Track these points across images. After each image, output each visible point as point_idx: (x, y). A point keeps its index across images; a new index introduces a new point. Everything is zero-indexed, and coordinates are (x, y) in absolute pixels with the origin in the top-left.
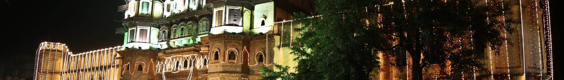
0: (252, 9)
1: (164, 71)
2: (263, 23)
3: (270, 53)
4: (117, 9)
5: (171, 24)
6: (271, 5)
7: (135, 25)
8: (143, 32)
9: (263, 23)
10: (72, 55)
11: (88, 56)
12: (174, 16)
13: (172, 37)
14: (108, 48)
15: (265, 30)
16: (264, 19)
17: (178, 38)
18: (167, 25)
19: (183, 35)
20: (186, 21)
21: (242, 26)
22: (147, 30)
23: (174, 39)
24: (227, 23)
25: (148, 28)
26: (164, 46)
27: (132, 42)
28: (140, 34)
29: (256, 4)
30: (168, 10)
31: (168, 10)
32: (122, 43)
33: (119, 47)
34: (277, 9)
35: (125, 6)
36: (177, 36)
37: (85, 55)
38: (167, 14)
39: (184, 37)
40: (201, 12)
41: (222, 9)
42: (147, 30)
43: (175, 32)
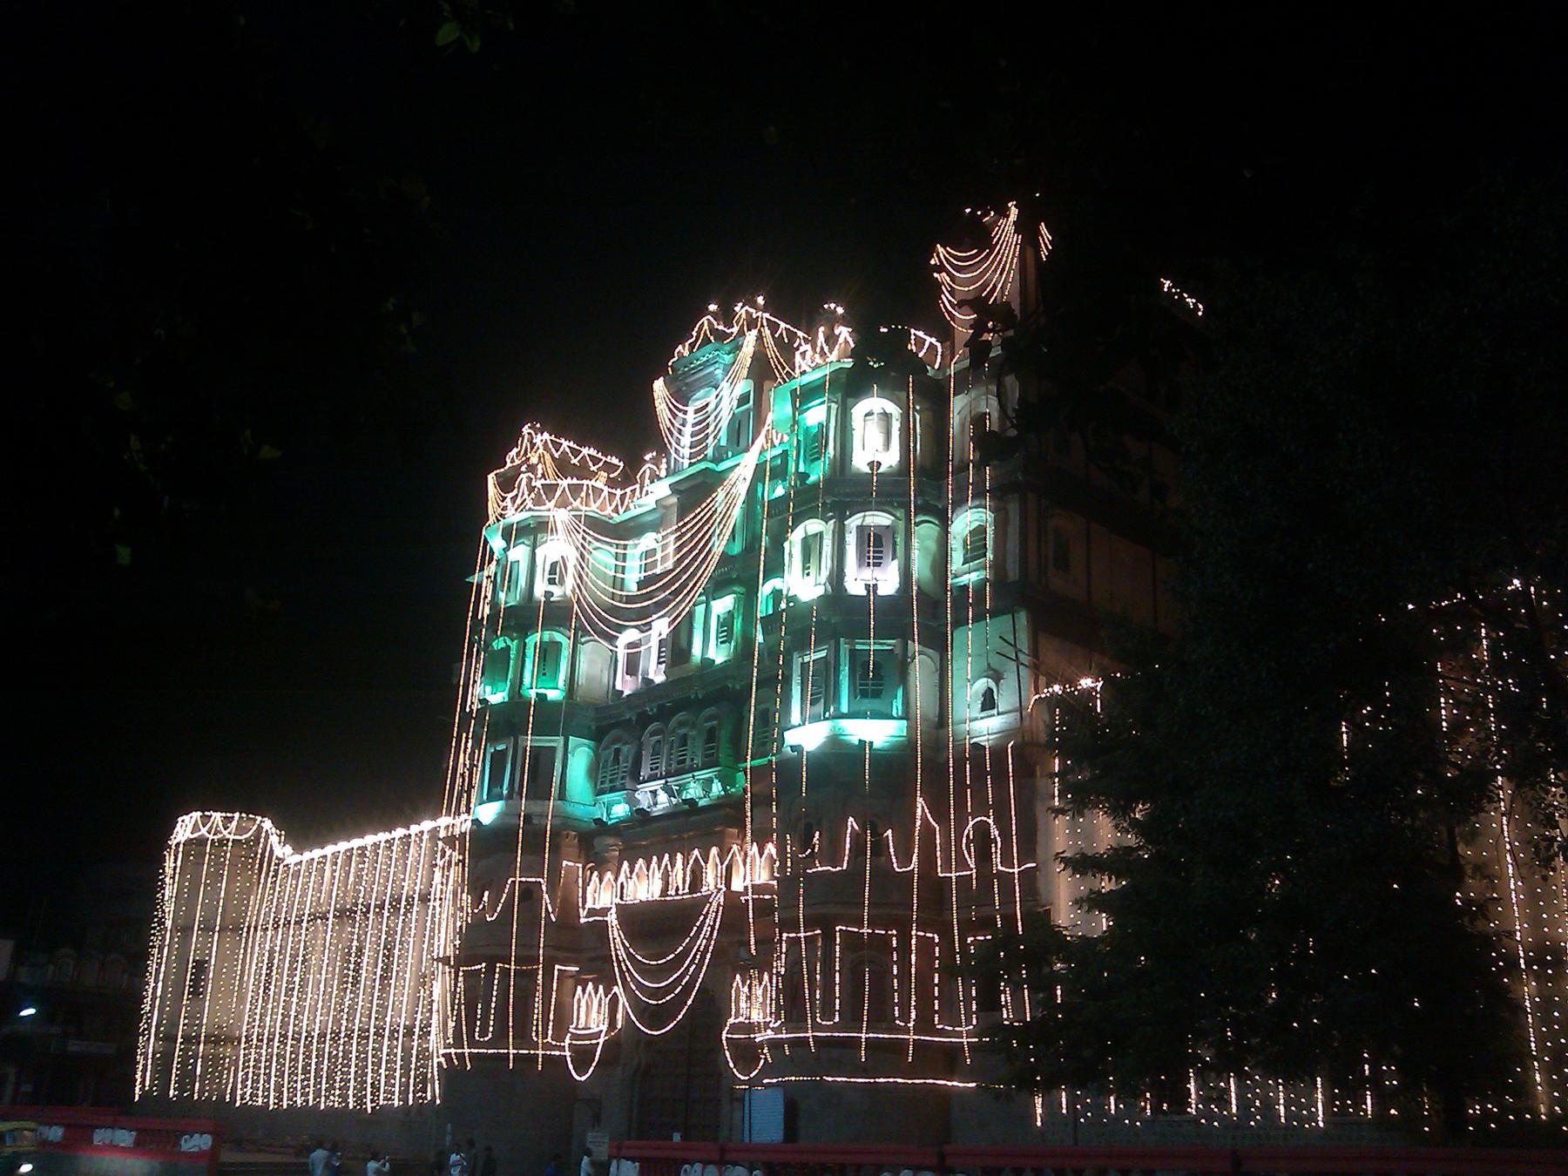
10: (292, 859)
16: (992, 685)
22: (554, 749)
42: (554, 749)
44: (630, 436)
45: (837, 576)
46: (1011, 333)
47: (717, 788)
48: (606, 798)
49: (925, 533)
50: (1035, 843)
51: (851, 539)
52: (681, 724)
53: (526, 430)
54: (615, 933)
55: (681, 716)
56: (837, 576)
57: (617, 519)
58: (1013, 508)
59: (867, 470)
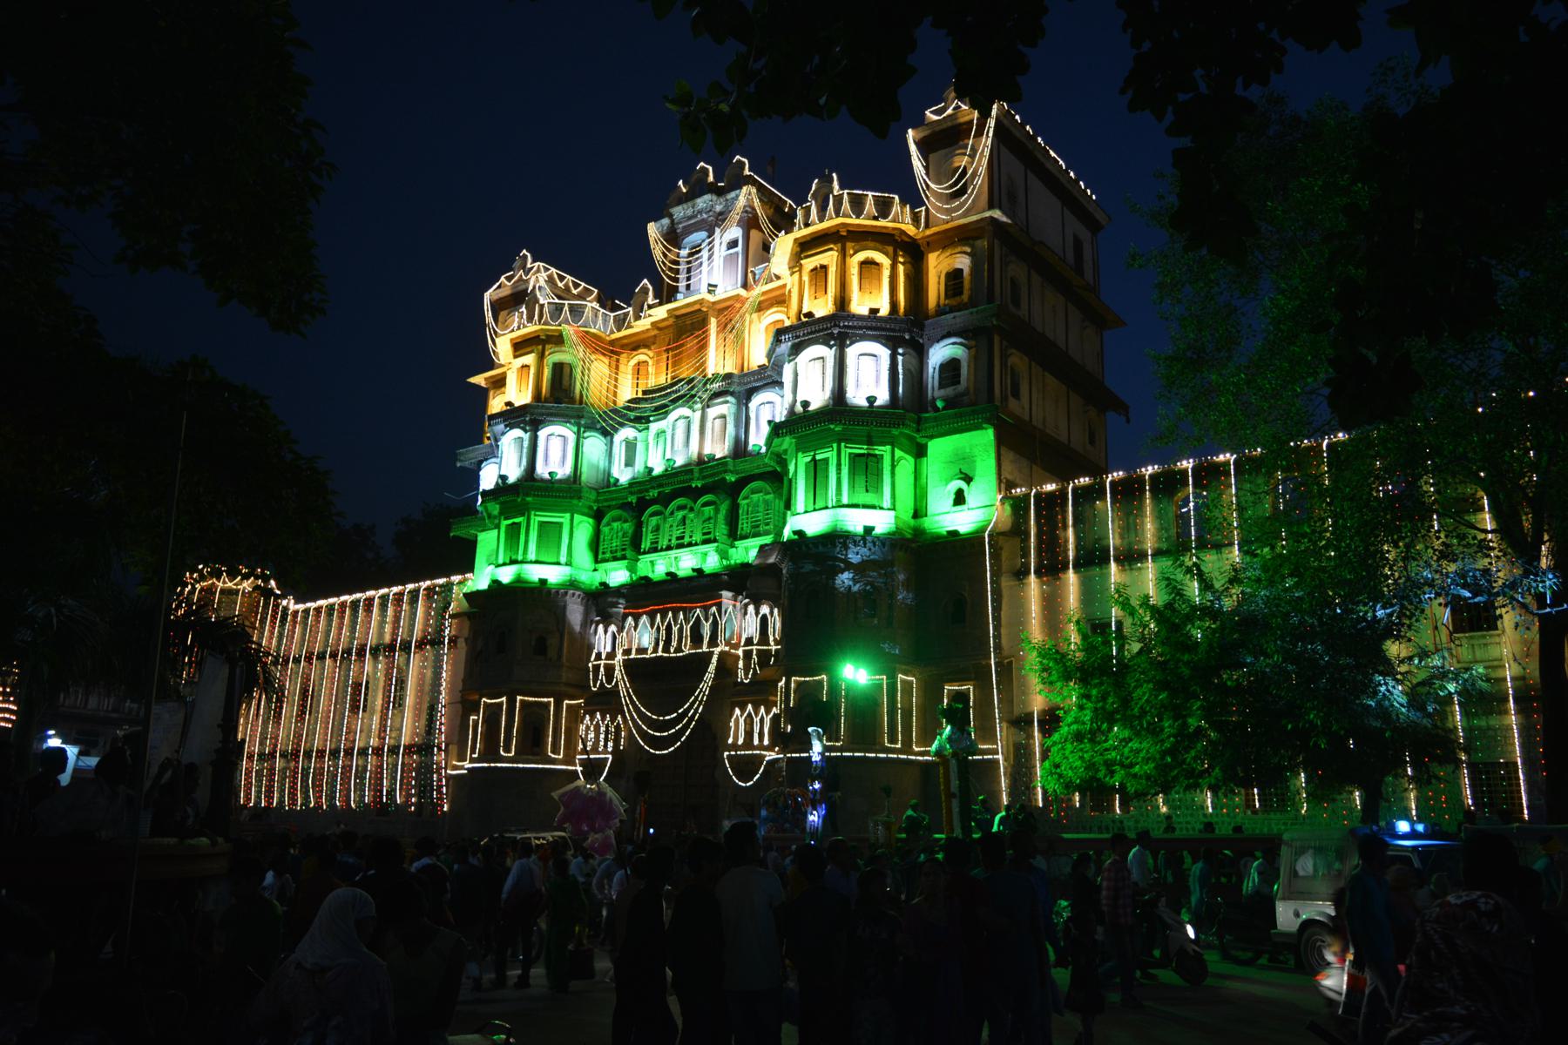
0: (920, 452)
1: (619, 657)
2: (959, 499)
3: (1017, 755)
4: (455, 458)
5: (643, 505)
6: (987, 436)
7: (524, 510)
8: (549, 533)
9: (959, 499)
10: (293, 607)
11: (294, 622)
12: (648, 481)
13: (646, 544)
14: (404, 584)
15: (963, 521)
16: (962, 484)
17: (669, 548)
18: (626, 506)
19: (687, 540)
20: (695, 494)
21: (569, 564)
22: (560, 525)
23: (654, 550)
24: (845, 501)
25: (564, 519)
26: (617, 575)
27: (513, 562)
28: (540, 536)
29: (932, 437)
30: (629, 462)
31: (629, 462)
32: (467, 566)
33: (456, 578)
34: (1003, 450)
35: (478, 450)
36: (664, 543)
37: (400, 595)
38: (623, 475)
39: (690, 545)
40: (746, 467)
41: (828, 454)
42: (560, 525)
43: (657, 529)
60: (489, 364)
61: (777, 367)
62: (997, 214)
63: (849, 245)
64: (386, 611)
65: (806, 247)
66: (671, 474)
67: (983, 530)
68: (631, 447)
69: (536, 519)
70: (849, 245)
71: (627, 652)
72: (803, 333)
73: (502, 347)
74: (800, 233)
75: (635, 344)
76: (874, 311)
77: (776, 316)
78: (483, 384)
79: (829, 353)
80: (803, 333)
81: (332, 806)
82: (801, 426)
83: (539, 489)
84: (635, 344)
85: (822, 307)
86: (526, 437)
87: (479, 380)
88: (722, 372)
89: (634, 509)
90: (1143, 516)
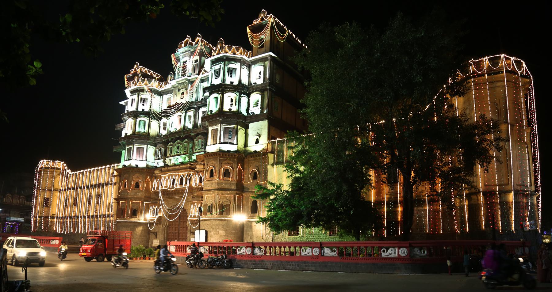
1: (160, 189)
2: (257, 142)
4: (115, 127)
5: (168, 142)
7: (132, 143)
9: (257, 142)
10: (70, 173)
11: (86, 174)
12: (170, 134)
13: (168, 155)
15: (258, 148)
16: (258, 137)
17: (174, 156)
18: (163, 143)
20: (182, 139)
21: (237, 144)
22: (143, 148)
23: (171, 156)
24: (222, 141)
26: (161, 164)
28: (137, 151)
29: (250, 122)
30: (165, 129)
31: (165, 129)
32: (119, 161)
36: (173, 154)
37: (83, 172)
38: (164, 133)
39: (180, 155)
41: (218, 127)
42: (143, 148)
44: (165, 70)
45: (224, 80)
46: (269, 223)
47: (187, 160)
48: (158, 161)
49: (244, 99)
50: (267, 175)
51: (226, 70)
52: (178, 143)
53: (135, 66)
54: (160, 194)
55: (178, 141)
56: (224, 80)
57: (161, 90)
58: (266, 94)
59: (229, 83)
60: (126, 98)
61: (205, 99)
62: (271, 54)
63: (226, 62)
64: (103, 174)
65: (214, 63)
66: (177, 133)
67: (145, 213)
68: (165, 124)
69: (136, 146)
70: (226, 62)
71: (162, 187)
72: (212, 89)
73: (127, 92)
74: (212, 58)
75: (168, 92)
76: (232, 83)
77: (206, 84)
78: (124, 104)
79: (219, 96)
80: (212, 89)
81: (81, 232)
82: (210, 118)
83: (136, 137)
84: (168, 92)
85: (217, 82)
86: (133, 121)
87: (122, 103)
88: (190, 101)
89: (165, 143)
90: (398, 207)
